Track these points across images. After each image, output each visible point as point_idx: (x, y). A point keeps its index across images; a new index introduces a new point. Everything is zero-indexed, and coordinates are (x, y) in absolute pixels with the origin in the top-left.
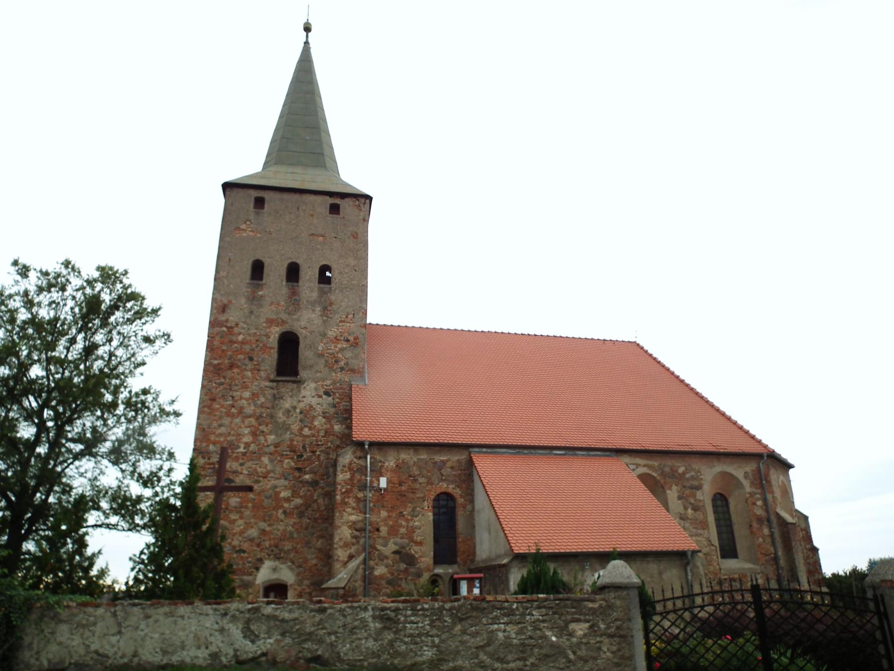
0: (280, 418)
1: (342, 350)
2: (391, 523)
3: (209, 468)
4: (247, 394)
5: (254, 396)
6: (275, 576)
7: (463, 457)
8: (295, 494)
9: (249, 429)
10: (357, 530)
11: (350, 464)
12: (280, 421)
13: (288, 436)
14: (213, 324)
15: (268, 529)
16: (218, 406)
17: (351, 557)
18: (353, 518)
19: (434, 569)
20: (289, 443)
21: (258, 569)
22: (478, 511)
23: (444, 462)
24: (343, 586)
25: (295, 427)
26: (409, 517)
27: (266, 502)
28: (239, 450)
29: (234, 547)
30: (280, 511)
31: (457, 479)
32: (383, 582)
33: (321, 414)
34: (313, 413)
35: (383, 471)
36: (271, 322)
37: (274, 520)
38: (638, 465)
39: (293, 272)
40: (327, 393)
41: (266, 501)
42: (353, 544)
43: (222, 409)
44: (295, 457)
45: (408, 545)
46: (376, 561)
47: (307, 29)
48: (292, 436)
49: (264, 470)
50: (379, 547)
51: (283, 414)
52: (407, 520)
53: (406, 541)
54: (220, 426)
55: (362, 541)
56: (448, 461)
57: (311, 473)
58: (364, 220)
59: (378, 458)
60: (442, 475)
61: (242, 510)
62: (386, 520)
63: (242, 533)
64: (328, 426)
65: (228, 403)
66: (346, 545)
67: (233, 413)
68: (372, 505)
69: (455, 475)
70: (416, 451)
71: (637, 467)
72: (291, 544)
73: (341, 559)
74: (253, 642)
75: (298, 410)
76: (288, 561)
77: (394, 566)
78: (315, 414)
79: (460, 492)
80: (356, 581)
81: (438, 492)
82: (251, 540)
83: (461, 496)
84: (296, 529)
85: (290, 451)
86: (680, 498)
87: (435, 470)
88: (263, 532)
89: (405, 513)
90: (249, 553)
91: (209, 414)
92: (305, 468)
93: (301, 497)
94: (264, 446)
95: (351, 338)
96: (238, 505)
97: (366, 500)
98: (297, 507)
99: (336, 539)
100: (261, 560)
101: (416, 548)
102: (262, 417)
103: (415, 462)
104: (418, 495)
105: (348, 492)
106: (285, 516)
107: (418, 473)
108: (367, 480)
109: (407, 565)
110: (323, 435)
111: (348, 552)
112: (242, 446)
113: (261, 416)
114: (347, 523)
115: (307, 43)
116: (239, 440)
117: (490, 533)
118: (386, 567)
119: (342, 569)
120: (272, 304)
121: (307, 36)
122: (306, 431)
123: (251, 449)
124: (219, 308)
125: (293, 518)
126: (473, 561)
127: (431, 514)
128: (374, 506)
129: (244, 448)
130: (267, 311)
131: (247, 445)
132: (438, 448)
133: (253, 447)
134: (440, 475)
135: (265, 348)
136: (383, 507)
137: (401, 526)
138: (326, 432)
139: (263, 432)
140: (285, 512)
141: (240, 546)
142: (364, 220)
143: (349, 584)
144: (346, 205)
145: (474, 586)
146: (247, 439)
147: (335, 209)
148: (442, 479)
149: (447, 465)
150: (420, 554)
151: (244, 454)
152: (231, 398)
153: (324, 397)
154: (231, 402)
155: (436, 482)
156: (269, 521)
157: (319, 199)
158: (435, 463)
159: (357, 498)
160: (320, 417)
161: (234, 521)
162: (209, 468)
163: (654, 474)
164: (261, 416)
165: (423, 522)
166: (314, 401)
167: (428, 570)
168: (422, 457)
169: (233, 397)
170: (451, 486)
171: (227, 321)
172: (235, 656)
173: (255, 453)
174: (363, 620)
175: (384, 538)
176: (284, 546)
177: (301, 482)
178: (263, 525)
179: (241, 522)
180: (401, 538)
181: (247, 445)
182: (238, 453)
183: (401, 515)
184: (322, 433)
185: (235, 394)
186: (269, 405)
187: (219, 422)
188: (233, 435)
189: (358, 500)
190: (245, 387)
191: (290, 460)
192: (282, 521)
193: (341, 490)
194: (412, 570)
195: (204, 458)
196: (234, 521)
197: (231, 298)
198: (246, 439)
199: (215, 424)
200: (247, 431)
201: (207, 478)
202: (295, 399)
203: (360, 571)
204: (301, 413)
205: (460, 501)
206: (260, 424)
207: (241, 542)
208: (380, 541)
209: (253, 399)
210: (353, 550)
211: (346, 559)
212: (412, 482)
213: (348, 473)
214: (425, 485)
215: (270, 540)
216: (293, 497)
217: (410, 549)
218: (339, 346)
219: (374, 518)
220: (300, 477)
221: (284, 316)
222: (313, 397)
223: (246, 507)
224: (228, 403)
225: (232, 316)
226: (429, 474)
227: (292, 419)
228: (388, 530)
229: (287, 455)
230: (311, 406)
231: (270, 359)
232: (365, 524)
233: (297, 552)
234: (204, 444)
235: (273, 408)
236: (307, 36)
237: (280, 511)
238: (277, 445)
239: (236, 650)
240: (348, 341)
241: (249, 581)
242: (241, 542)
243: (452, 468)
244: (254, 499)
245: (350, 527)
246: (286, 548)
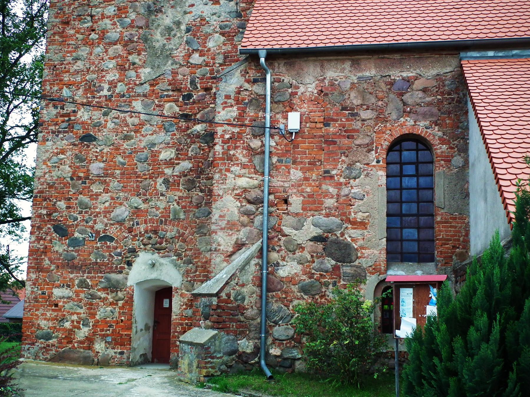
2: (308, 190)
4: (111, 10)
6: (153, 275)
7: (449, 69)
8: (181, 155)
9: (114, 61)
10: (249, 202)
11: (239, 92)
12: (157, 45)
13: (168, 67)
15: (143, 206)
16: (72, 32)
17: (239, 246)
18: (243, 182)
19: (387, 268)
20: (170, 78)
21: (130, 264)
22: (473, 165)
23: (409, 81)
24: (215, 292)
25: (180, 54)
26: (342, 180)
27: (141, 168)
28: (102, 93)
29: (98, 232)
30: (160, 180)
31: (435, 110)
32: (295, 288)
33: (218, 29)
34: (207, 29)
35: (296, 101)
37: (151, 194)
41: (139, 165)
42: (244, 225)
43: (77, 36)
44: (181, 99)
45: (340, 226)
46: (283, 253)
48: (175, 67)
49: (136, 121)
50: (287, 230)
51: (162, 35)
52: (339, 185)
53: (337, 220)
54: (76, 59)
55: (258, 219)
56: (416, 78)
57: (203, 122)
59: (287, 79)
60: (405, 104)
61: (108, 179)
62: (300, 185)
63: (107, 212)
64: (229, 48)
65: (86, 25)
66: (231, 226)
67: (93, 40)
68: (275, 159)
69: (429, 104)
70: (356, 64)
72: (175, 229)
73: (222, 248)
75: (183, 27)
76: (172, 254)
77: (313, 262)
78: (209, 30)
79: (440, 134)
80: (243, 285)
81: (397, 135)
82: (121, 223)
83: (442, 141)
84: (183, 207)
85: (173, 91)
87: (392, 96)
88: (137, 212)
89: (334, 172)
90: (117, 242)
92: (195, 115)
93: (190, 159)
94: (135, 84)
96: (101, 172)
97: (263, 152)
98: (184, 174)
99: (215, 216)
100: (134, 252)
101: (355, 233)
102: (133, 42)
103: (353, 84)
104: (358, 142)
105: (234, 139)
106: (168, 188)
107: (359, 102)
108: (265, 118)
109: (337, 260)
110: (221, 61)
111: (234, 237)
112: (106, 86)
113: (131, 41)
114: (234, 189)
116: (101, 79)
117: (486, 200)
118: (299, 263)
119: (225, 264)
123: (117, 90)
125: (179, 190)
126: (463, 256)
127: (382, 174)
128: (279, 161)
129: (109, 90)
131: (113, 85)
132: (397, 56)
133: (121, 88)
134: (401, 105)
136: (294, 162)
137: (327, 194)
138: (225, 58)
139: (134, 64)
140: (166, 182)
141: (105, 231)
143: (227, 290)
145: (428, 301)
148: (404, 112)
149: (414, 87)
150: (360, 242)
151: (109, 99)
152: (89, 18)
154: (90, 24)
155: (394, 116)
156: (145, 195)
158: (392, 84)
159: (249, 148)
160: (218, 35)
161: (98, 195)
164: (131, 41)
165: (368, 188)
167: (376, 270)
168: (367, 74)
169: (92, 16)
170: (422, 124)
173: (123, 96)
176: (167, 231)
177: (189, 136)
178: (136, 201)
179: (106, 197)
180: (327, 215)
181: (113, 85)
182: (100, 97)
183: (327, 176)
184: (220, 59)
185: (94, 11)
186: (142, 23)
187: (74, 54)
188: (93, 72)
189: (252, 152)
191: (173, 104)
192: (162, 195)
193: (222, 136)
194: (346, 269)
195: (55, 107)
196: (98, 195)
198: (110, 77)
199: (69, 59)
200: (111, 64)
201: (61, 136)
202: (179, 9)
203: (252, 268)
204: (188, 30)
205: (441, 149)
206: (130, 53)
207: (106, 225)
208: (288, 220)
209: (119, 17)
210: (242, 234)
211: (231, 249)
212: (347, 120)
213: (235, 108)
214: (372, 123)
215: (146, 222)
216: (178, 158)
217: (342, 234)
219: (277, 182)
220: (188, 128)
223: (112, 175)
224: (86, 25)
226: (380, 103)
227: (175, 41)
228: (303, 203)
229: (168, 96)
230: (203, 19)
232: (263, 191)
233: (184, 241)
234: (56, 88)
235: (147, 27)
237: (160, 180)
238: (154, 83)
241: (118, 282)
242: (106, 225)
243: (425, 90)
244: (124, 164)
246: (169, 235)
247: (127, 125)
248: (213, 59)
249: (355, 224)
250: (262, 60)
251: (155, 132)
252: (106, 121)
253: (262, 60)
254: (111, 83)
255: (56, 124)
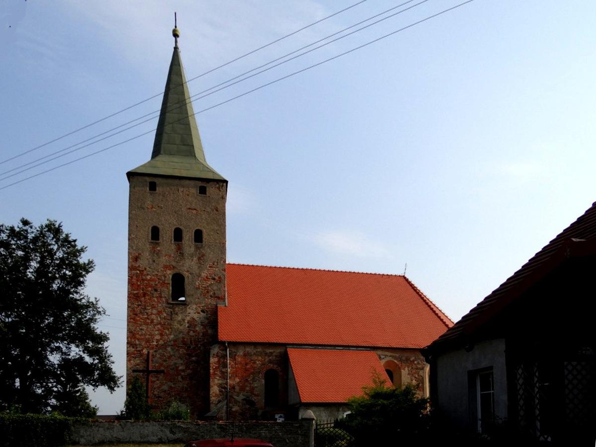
0: (176, 326)
1: (211, 284)
3: (137, 353)
4: (155, 311)
5: (159, 313)
8: (187, 367)
10: (222, 388)
11: (217, 353)
14: (131, 268)
15: (173, 386)
16: (139, 319)
29: (155, 395)
30: (180, 377)
32: (237, 414)
33: (200, 323)
36: (166, 267)
38: (386, 356)
39: (178, 235)
40: (203, 311)
41: (171, 371)
47: (176, 35)
49: (169, 355)
52: (250, 383)
58: (222, 198)
63: (159, 388)
64: (205, 330)
71: (385, 357)
74: (174, 435)
75: (186, 321)
85: (183, 344)
86: (409, 374)
91: (135, 323)
95: (216, 278)
98: (188, 375)
101: (255, 398)
103: (254, 353)
108: (227, 362)
115: (176, 48)
116: (153, 338)
118: (238, 406)
120: (166, 255)
121: (176, 42)
122: (191, 333)
124: (134, 258)
130: (164, 260)
131: (158, 341)
135: (164, 284)
140: (182, 377)
142: (222, 198)
144: (211, 190)
146: (158, 337)
147: (203, 191)
150: (257, 400)
151: (157, 346)
153: (201, 313)
154: (146, 316)
157: (192, 183)
162: (137, 353)
163: (396, 361)
166: (196, 316)
168: (259, 350)
169: (147, 313)
170: (275, 366)
171: (139, 266)
172: (168, 439)
174: (214, 428)
175: (238, 392)
179: (158, 382)
184: (201, 334)
185: (148, 311)
190: (153, 307)
191: (183, 349)
192: (181, 382)
195: (133, 347)
197: (140, 252)
204: (188, 323)
215: (175, 391)
218: (209, 283)
221: (174, 264)
222: (195, 313)
225: (143, 263)
229: (181, 346)
230: (194, 319)
231: (168, 291)
234: (133, 340)
236: (176, 42)
237: (180, 377)
238: (175, 341)
239: (167, 437)
240: (214, 279)
245: (218, 386)
247: (165, 356)
248: (199, 334)
249: (255, 395)
250: (227, 344)
251: (176, 359)
252: (156, 354)
253: (227, 344)
254: (157, 339)
255: (134, 354)
